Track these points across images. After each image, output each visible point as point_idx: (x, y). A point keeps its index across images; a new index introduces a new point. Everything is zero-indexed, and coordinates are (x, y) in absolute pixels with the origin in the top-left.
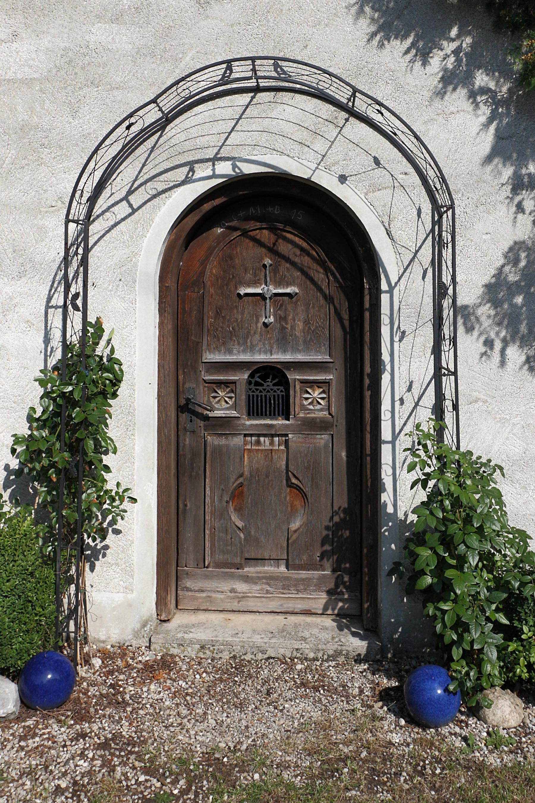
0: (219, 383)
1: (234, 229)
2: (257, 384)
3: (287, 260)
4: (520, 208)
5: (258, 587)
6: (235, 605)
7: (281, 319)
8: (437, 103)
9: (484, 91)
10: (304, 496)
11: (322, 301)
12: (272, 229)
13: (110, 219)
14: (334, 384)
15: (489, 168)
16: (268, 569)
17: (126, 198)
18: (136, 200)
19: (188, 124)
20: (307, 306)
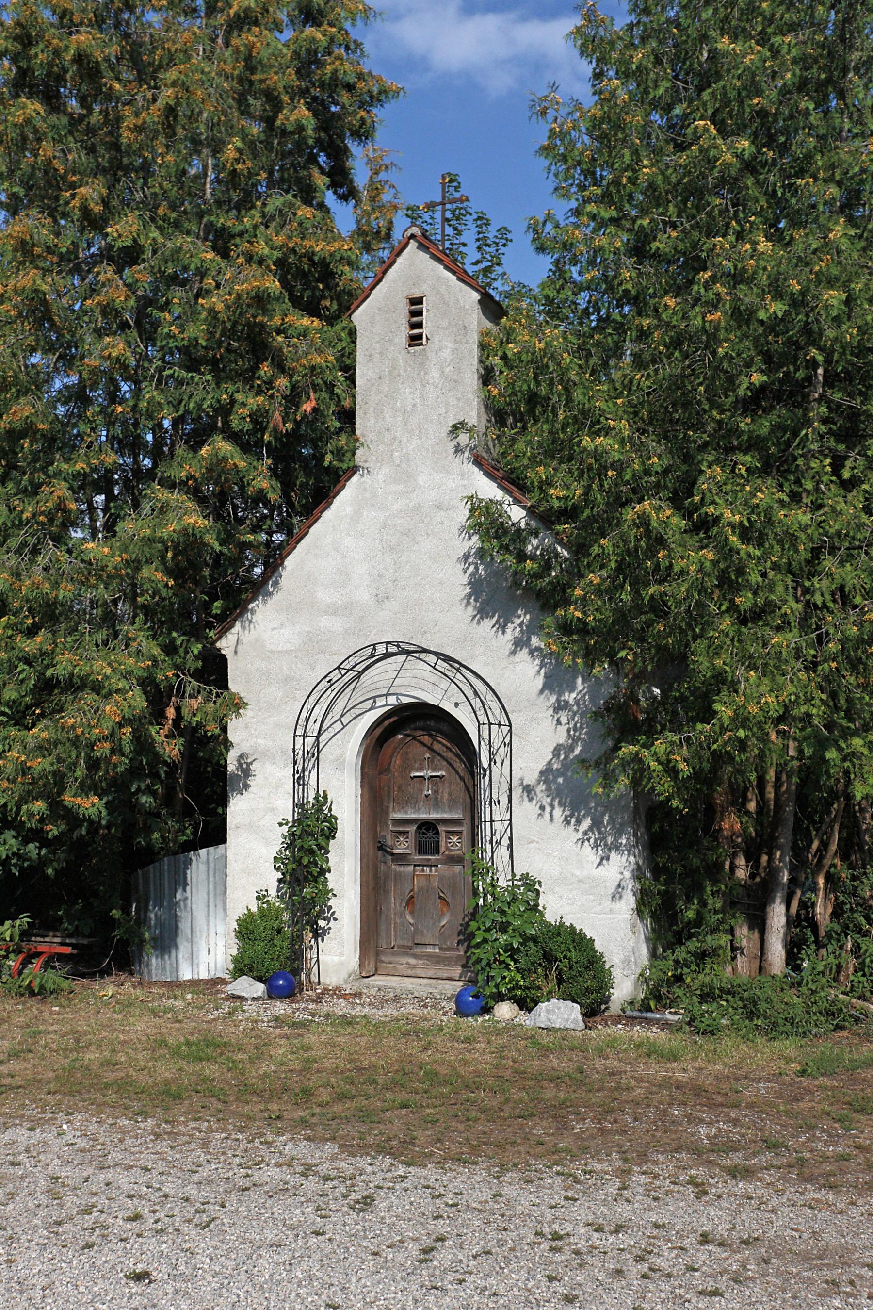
0: (400, 833)
1: (407, 735)
2: (424, 834)
3: (439, 754)
4: (559, 722)
5: (421, 962)
6: (410, 972)
7: (436, 792)
8: (512, 658)
9: (538, 649)
10: (448, 904)
11: (459, 780)
12: (430, 735)
13: (332, 731)
14: (465, 833)
15: (543, 696)
16: (429, 950)
17: (340, 719)
18: (345, 720)
19: (372, 674)
20: (450, 783)
